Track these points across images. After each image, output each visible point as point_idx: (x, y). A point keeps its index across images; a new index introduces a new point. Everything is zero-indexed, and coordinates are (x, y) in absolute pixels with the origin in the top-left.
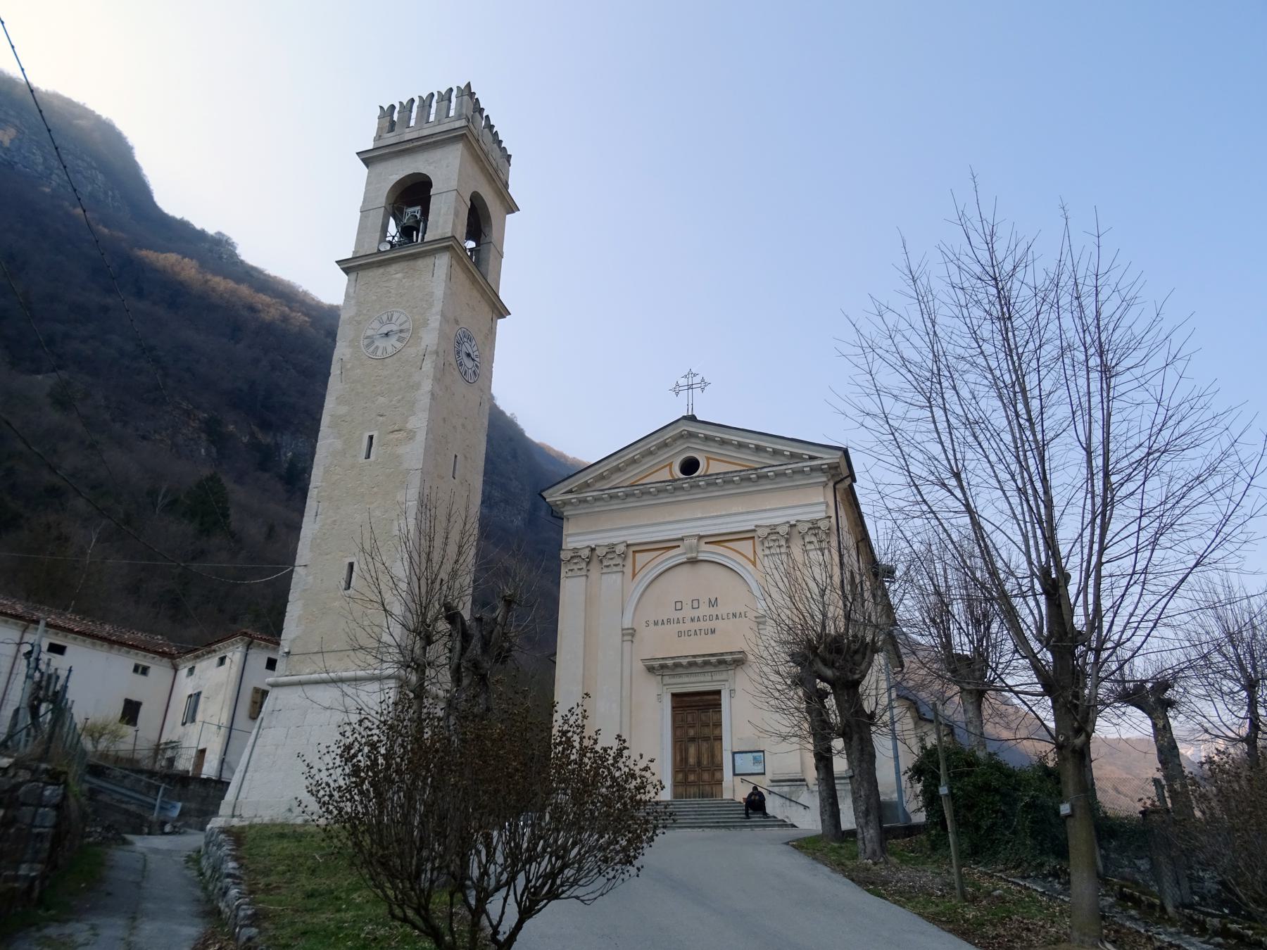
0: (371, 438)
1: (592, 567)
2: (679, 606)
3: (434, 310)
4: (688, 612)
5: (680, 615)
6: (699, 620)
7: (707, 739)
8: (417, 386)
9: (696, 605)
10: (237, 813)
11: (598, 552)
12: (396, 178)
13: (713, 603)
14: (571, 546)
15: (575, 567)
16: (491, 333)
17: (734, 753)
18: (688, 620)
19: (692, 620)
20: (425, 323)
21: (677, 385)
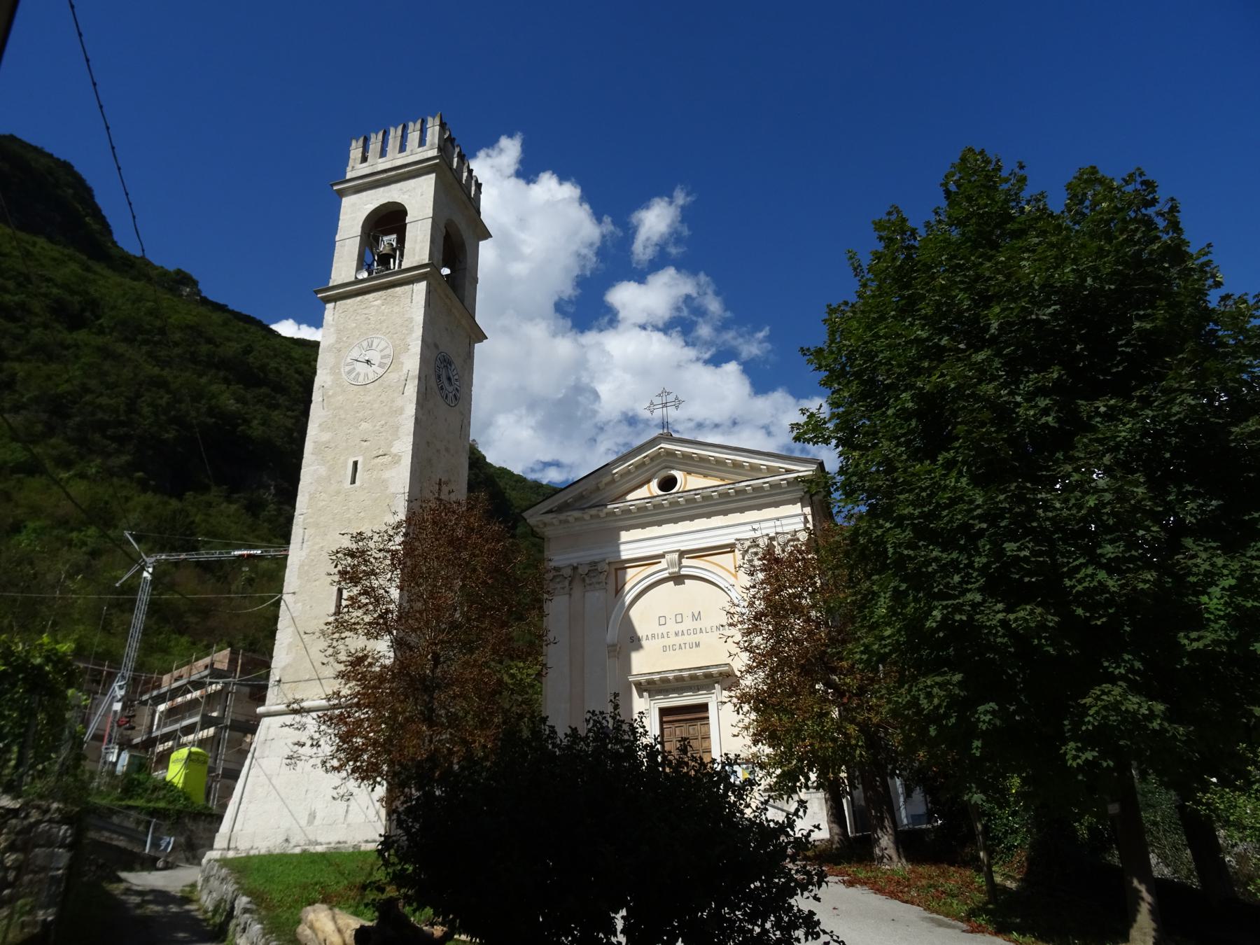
0: (356, 463)
2: (662, 621)
4: (672, 627)
5: (663, 629)
6: (683, 634)
8: (401, 411)
9: (679, 619)
10: (232, 845)
11: (580, 571)
12: (370, 207)
13: (696, 617)
16: (470, 356)
18: (672, 635)
19: (676, 634)
21: (652, 403)
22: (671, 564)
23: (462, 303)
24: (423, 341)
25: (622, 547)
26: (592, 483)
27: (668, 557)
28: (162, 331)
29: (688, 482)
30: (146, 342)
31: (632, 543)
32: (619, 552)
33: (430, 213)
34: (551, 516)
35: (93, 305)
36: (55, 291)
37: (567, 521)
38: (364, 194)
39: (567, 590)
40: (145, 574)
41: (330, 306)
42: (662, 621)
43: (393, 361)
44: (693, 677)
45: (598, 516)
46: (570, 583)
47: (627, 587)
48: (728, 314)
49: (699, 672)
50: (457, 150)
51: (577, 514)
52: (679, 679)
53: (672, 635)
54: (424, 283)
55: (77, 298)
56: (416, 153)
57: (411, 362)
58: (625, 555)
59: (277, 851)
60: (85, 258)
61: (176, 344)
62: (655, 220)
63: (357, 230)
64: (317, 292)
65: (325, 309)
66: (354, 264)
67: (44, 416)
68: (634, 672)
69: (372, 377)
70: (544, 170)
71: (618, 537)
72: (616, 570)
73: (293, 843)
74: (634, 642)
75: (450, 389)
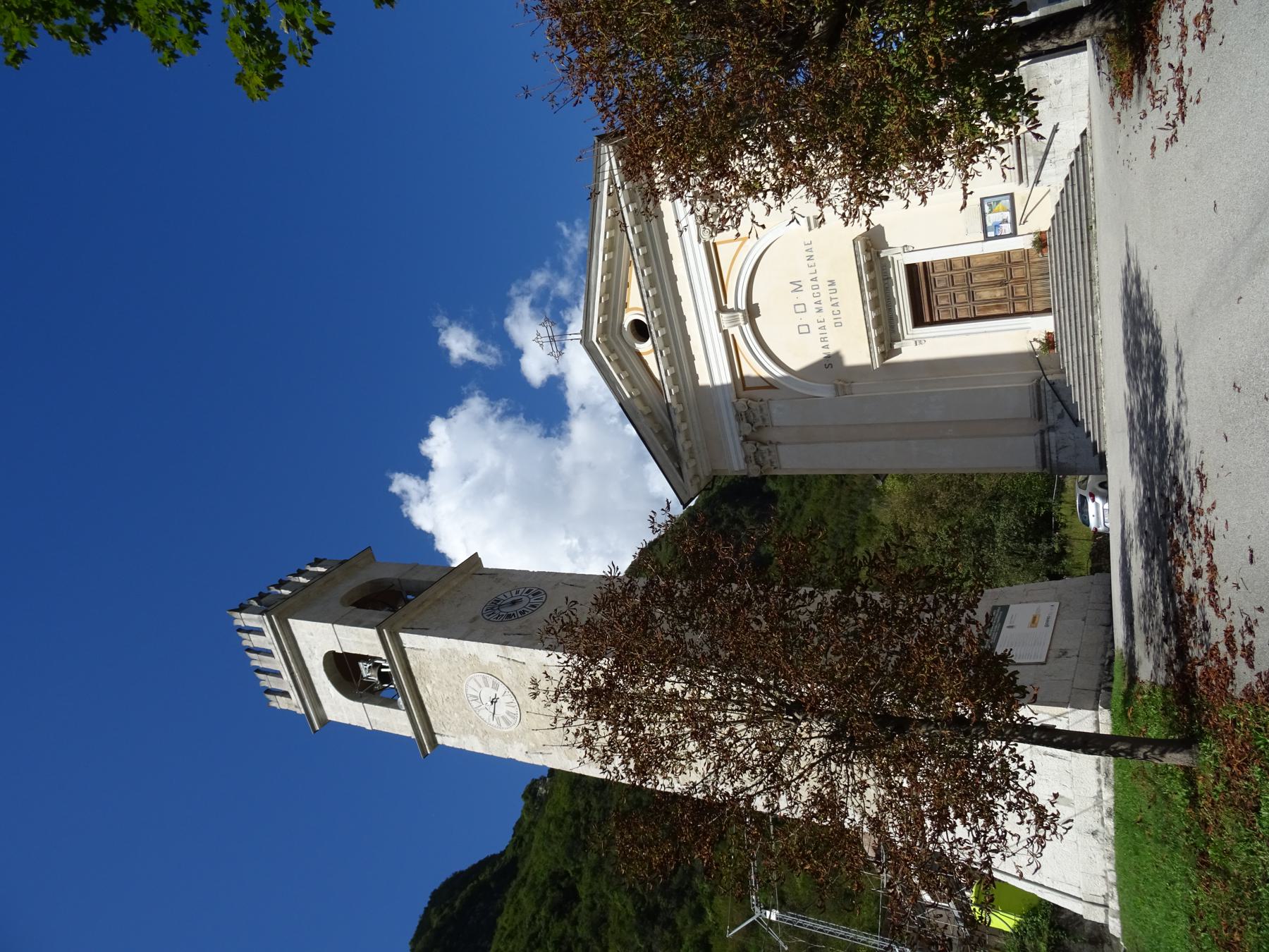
1: (765, 438)
2: (804, 329)
3: (459, 649)
4: (811, 317)
5: (815, 328)
6: (819, 302)
7: (969, 277)
9: (801, 308)
10: (1101, 901)
11: (747, 432)
13: (797, 286)
14: (743, 466)
15: (768, 458)
16: (496, 574)
17: (987, 239)
18: (821, 316)
20: (474, 657)
22: (734, 322)
23: (433, 584)
24: (463, 638)
25: (717, 382)
26: (642, 422)
27: (725, 326)
28: (576, 815)
29: (635, 309)
30: (587, 831)
31: (713, 370)
32: (723, 386)
33: (327, 627)
34: (685, 470)
35: (556, 878)
36: (543, 913)
37: (691, 450)
38: (320, 696)
39: (769, 447)
40: (773, 918)
41: (440, 740)
42: (803, 330)
43: (489, 673)
44: (873, 286)
45: (682, 413)
46: (765, 444)
47: (765, 374)
48: (547, 263)
49: (866, 278)
50: (273, 589)
51: (681, 439)
52: (875, 304)
53: (821, 316)
54: (403, 636)
55: (548, 893)
56: (267, 640)
57: (488, 652)
58: (727, 379)
59: (1111, 848)
60: (514, 883)
61: (588, 803)
62: (460, 344)
63: (357, 706)
64: (425, 755)
65: (443, 746)
66: (393, 711)
67: (657, 929)
68: (867, 361)
69: (510, 698)
70: (419, 451)
71: (706, 388)
72: (745, 389)
73: (1098, 826)
74: (832, 362)
75: (525, 600)
